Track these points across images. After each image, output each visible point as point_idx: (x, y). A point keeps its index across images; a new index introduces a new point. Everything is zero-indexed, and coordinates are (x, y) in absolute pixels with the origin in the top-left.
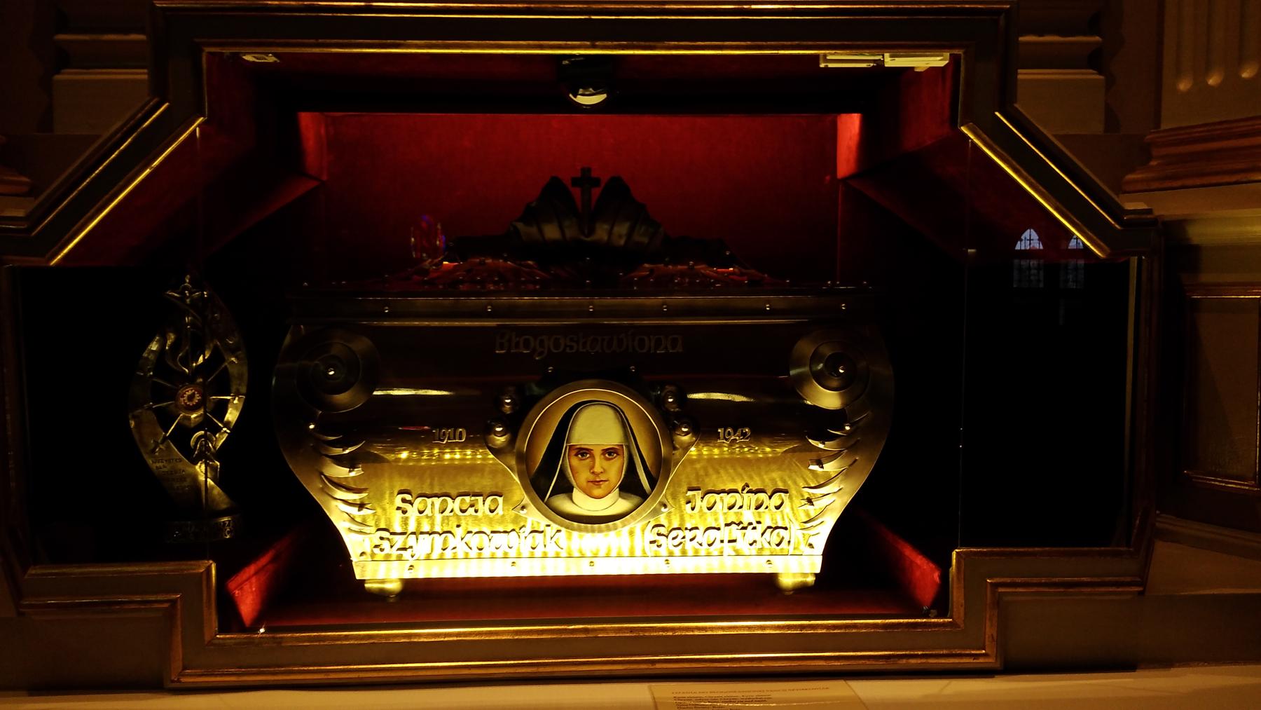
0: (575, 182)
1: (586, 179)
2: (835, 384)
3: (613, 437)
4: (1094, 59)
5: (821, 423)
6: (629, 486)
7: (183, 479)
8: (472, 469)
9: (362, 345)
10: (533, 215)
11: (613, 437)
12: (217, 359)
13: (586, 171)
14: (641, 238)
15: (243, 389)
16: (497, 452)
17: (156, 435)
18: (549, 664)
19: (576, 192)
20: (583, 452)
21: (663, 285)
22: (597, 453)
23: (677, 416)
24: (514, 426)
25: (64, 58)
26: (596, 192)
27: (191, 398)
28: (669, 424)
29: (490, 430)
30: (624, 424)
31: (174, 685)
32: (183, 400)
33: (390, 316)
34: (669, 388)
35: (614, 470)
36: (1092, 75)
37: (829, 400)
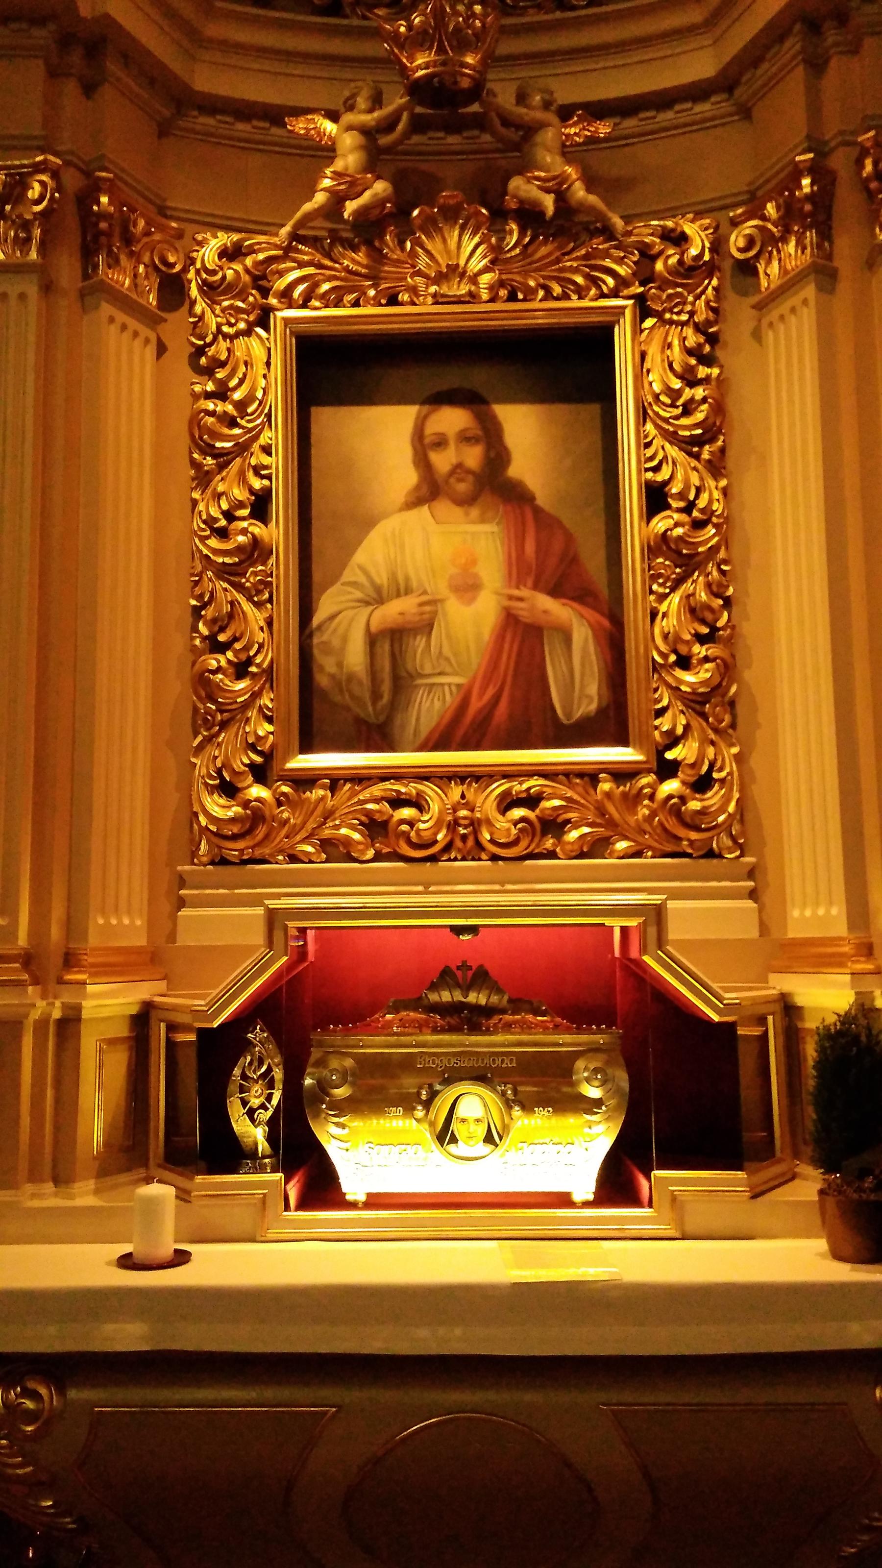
0: (458, 968)
1: (464, 966)
2: (596, 1083)
3: (480, 1113)
4: (753, 895)
5: (592, 1106)
6: (489, 1139)
7: (249, 1137)
8: (404, 1131)
9: (349, 1063)
10: (434, 987)
11: (480, 1113)
12: (269, 1070)
13: (464, 962)
14: (495, 999)
15: (281, 1087)
16: (418, 1120)
17: (239, 1111)
18: (386, 319)
19: (459, 974)
20: (463, 1121)
21: (508, 1027)
22: (471, 1121)
23: (513, 1101)
24: (427, 1105)
25: (182, 903)
26: (470, 974)
27: (256, 1092)
28: (509, 1105)
29: (414, 1109)
30: (485, 1105)
31: (263, 1239)
32: (253, 1092)
33: (362, 1047)
34: (510, 1086)
35: (482, 1131)
36: (750, 904)
37: (593, 1092)
